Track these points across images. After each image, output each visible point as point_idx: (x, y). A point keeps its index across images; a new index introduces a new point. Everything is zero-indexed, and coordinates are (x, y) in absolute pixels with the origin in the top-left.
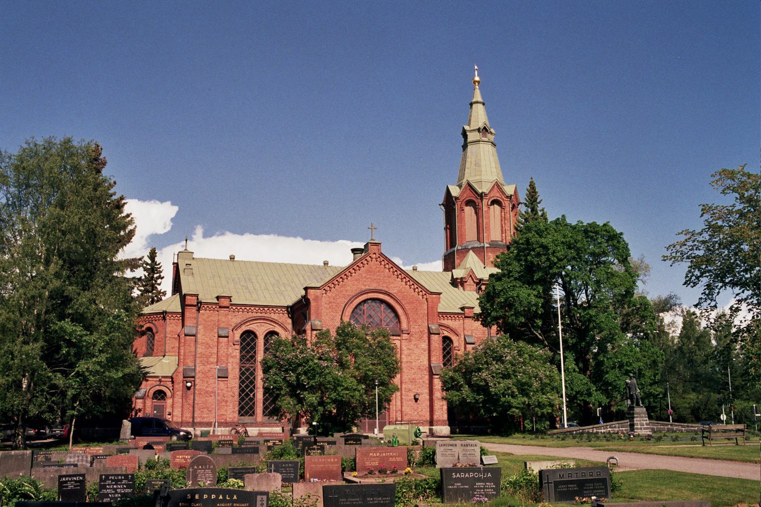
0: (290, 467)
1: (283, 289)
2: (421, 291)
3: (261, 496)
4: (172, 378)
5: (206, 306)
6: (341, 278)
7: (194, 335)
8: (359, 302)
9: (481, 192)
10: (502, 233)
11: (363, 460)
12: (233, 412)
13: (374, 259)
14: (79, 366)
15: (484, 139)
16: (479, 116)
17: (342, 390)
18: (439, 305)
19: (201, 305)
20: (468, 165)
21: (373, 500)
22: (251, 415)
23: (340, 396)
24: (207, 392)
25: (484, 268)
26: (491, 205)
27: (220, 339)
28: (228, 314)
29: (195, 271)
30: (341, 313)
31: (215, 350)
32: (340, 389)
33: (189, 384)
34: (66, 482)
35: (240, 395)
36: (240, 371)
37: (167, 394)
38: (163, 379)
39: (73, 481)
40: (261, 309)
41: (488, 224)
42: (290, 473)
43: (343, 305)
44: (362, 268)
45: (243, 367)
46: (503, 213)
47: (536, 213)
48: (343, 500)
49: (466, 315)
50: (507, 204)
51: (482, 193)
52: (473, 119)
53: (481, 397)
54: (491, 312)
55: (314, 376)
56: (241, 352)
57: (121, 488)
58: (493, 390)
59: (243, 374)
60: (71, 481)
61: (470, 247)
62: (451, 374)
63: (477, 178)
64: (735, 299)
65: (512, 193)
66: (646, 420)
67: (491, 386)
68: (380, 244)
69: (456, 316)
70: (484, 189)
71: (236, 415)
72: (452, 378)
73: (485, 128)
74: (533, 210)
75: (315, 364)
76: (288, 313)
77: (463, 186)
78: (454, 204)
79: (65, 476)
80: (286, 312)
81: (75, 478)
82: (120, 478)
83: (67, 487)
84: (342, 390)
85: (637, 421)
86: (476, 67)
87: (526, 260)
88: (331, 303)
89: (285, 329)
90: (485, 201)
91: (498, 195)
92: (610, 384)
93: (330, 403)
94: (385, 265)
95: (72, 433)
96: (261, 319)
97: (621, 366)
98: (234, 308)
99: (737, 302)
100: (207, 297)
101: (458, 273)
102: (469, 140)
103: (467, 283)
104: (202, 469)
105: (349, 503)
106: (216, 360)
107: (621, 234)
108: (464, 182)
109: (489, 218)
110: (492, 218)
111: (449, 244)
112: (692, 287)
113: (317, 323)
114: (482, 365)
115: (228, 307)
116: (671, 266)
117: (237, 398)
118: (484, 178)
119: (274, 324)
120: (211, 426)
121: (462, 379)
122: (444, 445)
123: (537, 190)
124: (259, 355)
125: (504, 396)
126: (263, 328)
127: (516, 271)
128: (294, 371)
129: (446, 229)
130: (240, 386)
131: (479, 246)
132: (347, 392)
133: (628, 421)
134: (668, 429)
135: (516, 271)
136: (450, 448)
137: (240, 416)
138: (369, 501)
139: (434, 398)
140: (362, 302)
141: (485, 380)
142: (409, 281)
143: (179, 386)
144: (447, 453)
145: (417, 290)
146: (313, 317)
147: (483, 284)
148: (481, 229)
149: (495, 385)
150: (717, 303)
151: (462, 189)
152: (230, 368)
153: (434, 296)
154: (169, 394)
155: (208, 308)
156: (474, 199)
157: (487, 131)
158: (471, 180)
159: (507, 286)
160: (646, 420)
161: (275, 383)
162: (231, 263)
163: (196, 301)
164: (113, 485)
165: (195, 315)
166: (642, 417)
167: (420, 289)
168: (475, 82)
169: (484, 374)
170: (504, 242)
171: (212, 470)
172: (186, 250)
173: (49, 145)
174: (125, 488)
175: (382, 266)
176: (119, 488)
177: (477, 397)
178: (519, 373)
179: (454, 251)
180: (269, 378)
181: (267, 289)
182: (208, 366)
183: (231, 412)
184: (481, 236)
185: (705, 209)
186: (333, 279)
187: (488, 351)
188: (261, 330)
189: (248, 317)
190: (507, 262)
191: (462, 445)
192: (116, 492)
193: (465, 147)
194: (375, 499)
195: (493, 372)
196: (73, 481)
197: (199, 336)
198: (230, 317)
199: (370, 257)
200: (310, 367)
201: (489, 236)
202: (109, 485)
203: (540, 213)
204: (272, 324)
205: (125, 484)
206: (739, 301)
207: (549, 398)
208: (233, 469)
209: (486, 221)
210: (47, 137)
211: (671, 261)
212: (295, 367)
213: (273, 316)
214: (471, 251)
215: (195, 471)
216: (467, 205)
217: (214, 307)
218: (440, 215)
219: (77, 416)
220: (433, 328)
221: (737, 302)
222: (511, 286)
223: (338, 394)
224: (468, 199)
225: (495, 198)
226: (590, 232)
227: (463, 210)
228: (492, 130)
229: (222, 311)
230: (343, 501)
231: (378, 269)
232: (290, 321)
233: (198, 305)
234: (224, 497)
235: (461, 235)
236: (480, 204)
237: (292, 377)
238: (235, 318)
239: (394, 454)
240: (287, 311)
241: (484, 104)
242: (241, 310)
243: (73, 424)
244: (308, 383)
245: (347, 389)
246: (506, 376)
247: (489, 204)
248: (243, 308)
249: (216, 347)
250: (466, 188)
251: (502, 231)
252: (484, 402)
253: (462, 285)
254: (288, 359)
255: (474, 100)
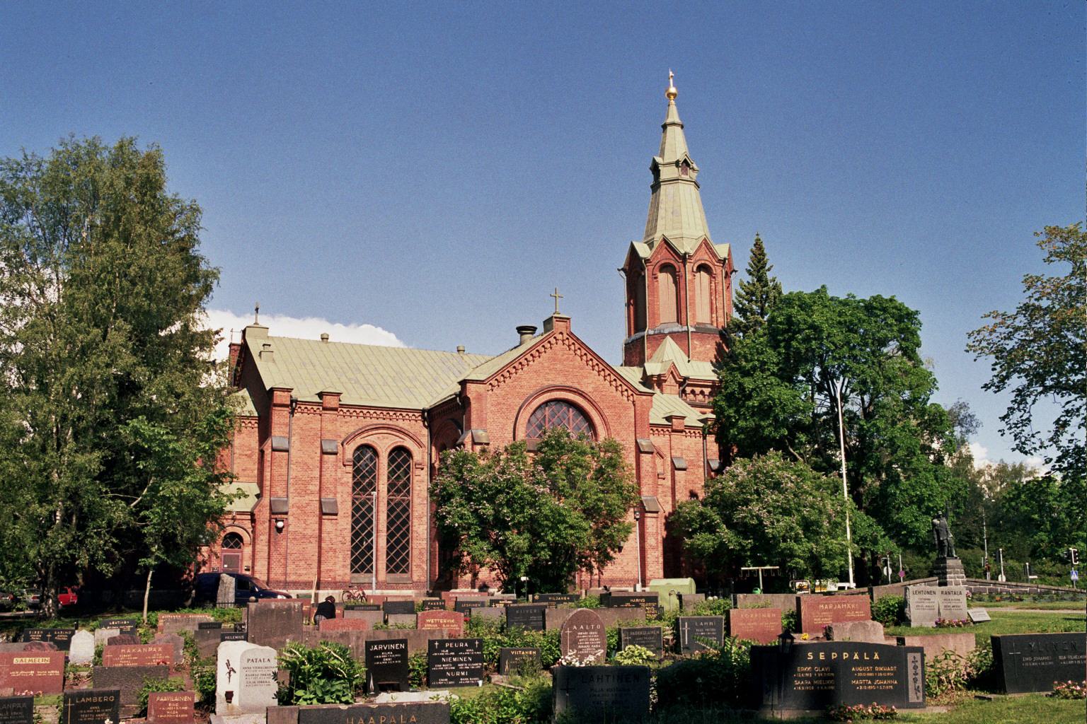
0: (711, 627)
1: (408, 384)
2: (626, 390)
3: (913, 654)
4: (252, 514)
5: (303, 407)
6: (514, 367)
7: (287, 451)
8: (538, 404)
9: (683, 252)
10: (712, 313)
11: (811, 615)
12: (344, 566)
13: (560, 342)
14: (163, 489)
15: (684, 177)
16: (676, 145)
17: (565, 528)
18: (652, 410)
19: (296, 404)
20: (661, 212)
21: (1067, 660)
22: (404, 572)
23: (562, 538)
24: (304, 536)
25: (689, 361)
26: (696, 272)
27: (325, 456)
28: (336, 420)
29: (275, 356)
30: (514, 419)
31: (317, 475)
32: (561, 527)
33: (280, 524)
34: (379, 652)
35: (353, 541)
36: (353, 505)
37: (245, 539)
38: (238, 517)
39: (390, 651)
40: (385, 413)
41: (693, 297)
42: (711, 636)
43: (518, 408)
44: (543, 354)
45: (357, 499)
46: (713, 284)
47: (766, 285)
48: (1027, 659)
49: (674, 427)
50: (718, 270)
51: (685, 254)
52: (667, 147)
53: (749, 543)
54: (737, 421)
55: (523, 508)
56: (354, 477)
57: (464, 662)
58: (770, 531)
59: (356, 509)
60: (387, 650)
61: (666, 332)
62: (701, 508)
63: (675, 232)
64: (1063, 410)
65: (726, 256)
66: (963, 577)
67: (766, 526)
68: (568, 319)
69: (660, 429)
70: (685, 247)
71: (348, 571)
72: (701, 514)
73: (685, 161)
74: (760, 279)
75: (525, 490)
76: (424, 419)
77: (656, 245)
78: (643, 269)
79: (378, 643)
80: (420, 418)
81: (392, 646)
82: (461, 645)
83: (381, 660)
84: (565, 528)
85: (951, 578)
86: (671, 74)
87: (788, 347)
88: (499, 404)
89: (420, 445)
90: (689, 266)
91: (706, 257)
92: (905, 527)
93: (545, 547)
94: (575, 350)
95: (147, 593)
96: (383, 428)
97: (920, 501)
98: (345, 410)
99: (1064, 414)
100: (305, 393)
101: (653, 368)
102: (663, 176)
103: (667, 383)
104: (585, 630)
105: (1036, 664)
106: (317, 488)
107: (917, 313)
108: (658, 237)
109: (694, 290)
110: (698, 291)
111: (632, 326)
112: (995, 392)
113: (480, 432)
114: (751, 495)
115: (336, 409)
116: (975, 360)
117: (348, 545)
118: (686, 233)
119: (403, 436)
120: (312, 588)
121: (718, 517)
122: (919, 592)
123: (765, 252)
124: (381, 482)
125: (785, 541)
126: (386, 441)
127: (773, 363)
128: (491, 500)
129: (628, 305)
130: (353, 528)
131: (680, 330)
132: (572, 532)
133: (937, 578)
134: (989, 589)
135: (773, 363)
136: (927, 596)
137: (389, 572)
138: (1061, 661)
139: (647, 546)
140: (543, 403)
141: (758, 517)
142: (609, 375)
143: (263, 527)
144: (925, 605)
145: (620, 388)
146: (474, 425)
147: (689, 385)
148: (683, 306)
149: (772, 523)
150: (1031, 415)
151: (654, 249)
152: (339, 499)
153: (644, 397)
154: (247, 538)
155: (306, 410)
156: (674, 263)
157: (688, 165)
158: (670, 234)
159: (762, 383)
160: (963, 577)
161: (461, 519)
162: (323, 345)
163: (289, 399)
164: (452, 656)
165: (287, 420)
166: (957, 573)
167: (625, 388)
168: (669, 95)
169: (755, 508)
170: (715, 325)
171: (599, 631)
172: (256, 323)
173: (93, 148)
174: (472, 662)
175: (572, 352)
176: (461, 662)
177: (744, 542)
178: (804, 507)
179: (643, 337)
180: (450, 511)
181: (386, 384)
182: (307, 497)
183: (339, 565)
184: (683, 315)
185: (1030, 282)
186: (502, 369)
187: (759, 475)
188: (384, 444)
189: (365, 424)
190: (757, 349)
191: (942, 593)
192: (457, 669)
193: (656, 187)
194: (1070, 657)
195: (768, 506)
196: (390, 651)
197: (292, 451)
198: (338, 424)
199: (555, 338)
200: (517, 494)
201: (694, 316)
202: (445, 656)
203: (771, 284)
204: (401, 435)
205: (470, 655)
206: (1067, 412)
207: (841, 545)
208: (629, 630)
209: (691, 294)
210: (90, 138)
211: (976, 354)
212: (492, 495)
213: (401, 424)
214: (668, 338)
215: (574, 633)
216: (661, 271)
217: (315, 408)
218: (620, 284)
219: (154, 567)
220: (644, 443)
221: (1064, 414)
222: (768, 384)
223: (558, 535)
224: (663, 262)
225: (703, 262)
226: (873, 308)
227: (656, 278)
228: (695, 166)
229: (328, 415)
230: (1028, 661)
231: (565, 356)
232: (425, 432)
233: (291, 405)
234: (861, 656)
235: (654, 314)
236: (682, 269)
237: (488, 510)
238: (347, 425)
239: (853, 606)
240: (423, 416)
241: (682, 127)
242: (355, 414)
243: (149, 579)
244: (513, 519)
245: (572, 527)
246: (787, 512)
247: (695, 270)
248: (358, 411)
249: (318, 469)
250: (660, 246)
251: (712, 309)
252: (753, 549)
253: (660, 386)
254: (482, 483)
255: (669, 121)
